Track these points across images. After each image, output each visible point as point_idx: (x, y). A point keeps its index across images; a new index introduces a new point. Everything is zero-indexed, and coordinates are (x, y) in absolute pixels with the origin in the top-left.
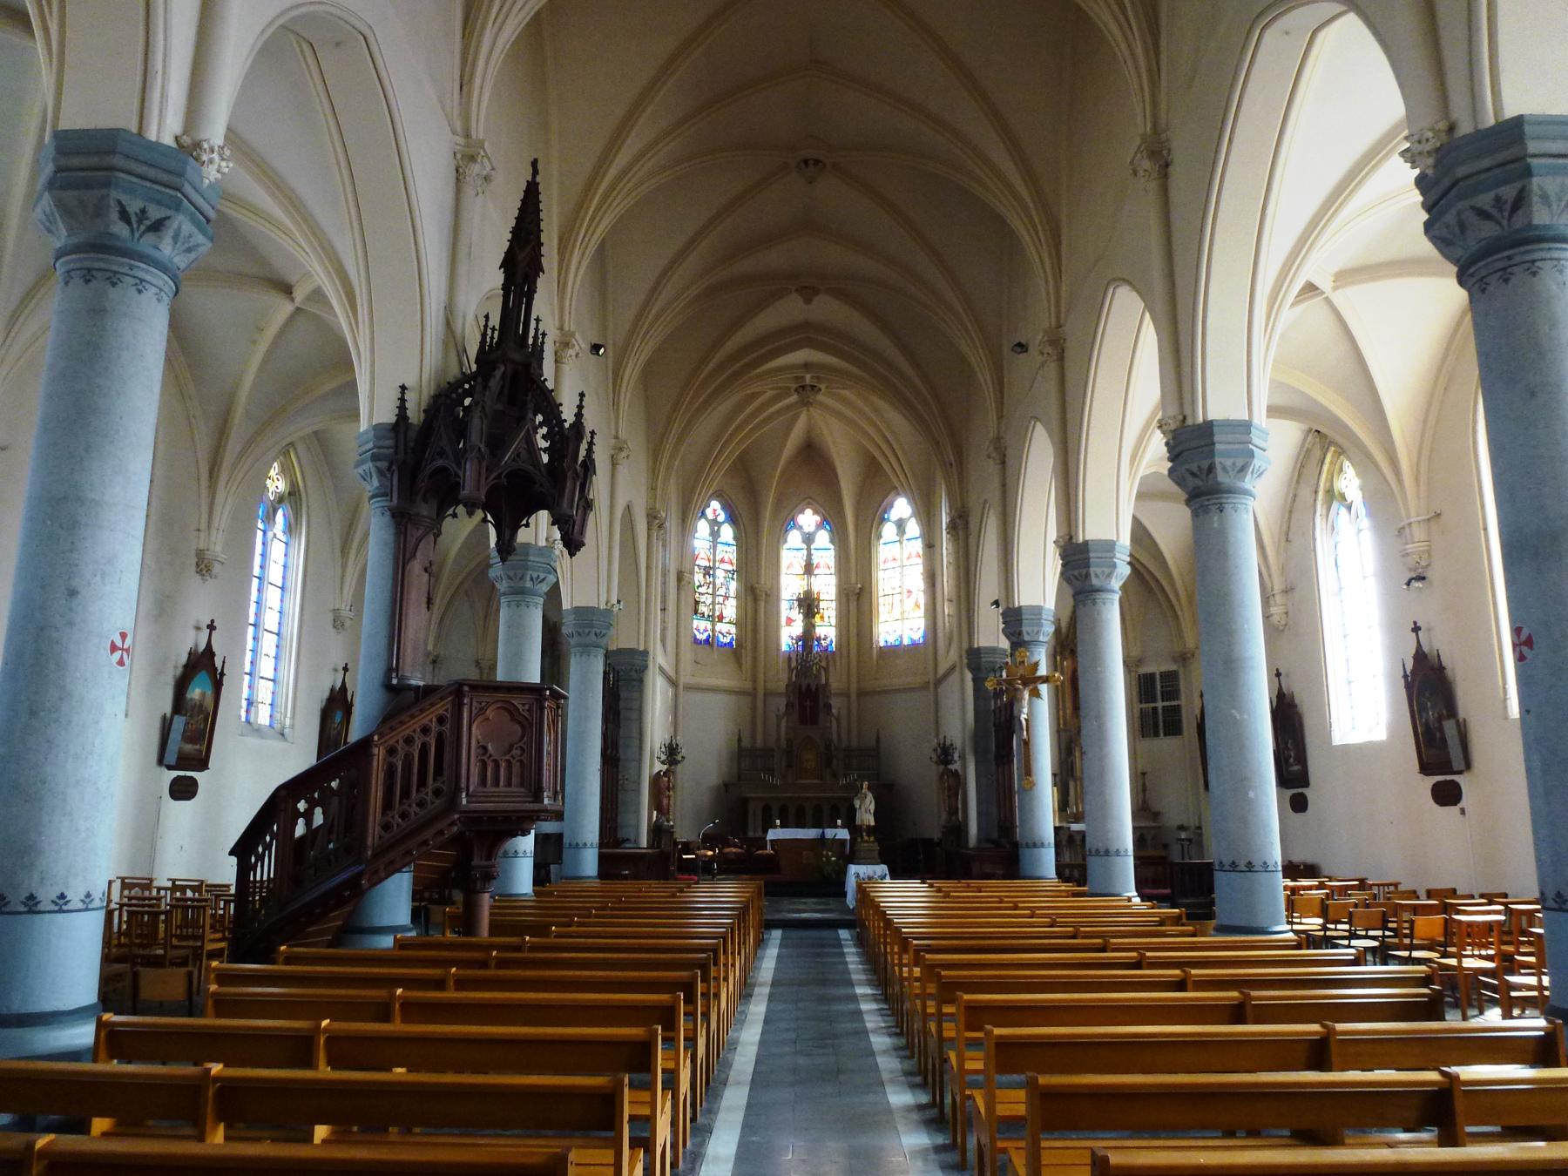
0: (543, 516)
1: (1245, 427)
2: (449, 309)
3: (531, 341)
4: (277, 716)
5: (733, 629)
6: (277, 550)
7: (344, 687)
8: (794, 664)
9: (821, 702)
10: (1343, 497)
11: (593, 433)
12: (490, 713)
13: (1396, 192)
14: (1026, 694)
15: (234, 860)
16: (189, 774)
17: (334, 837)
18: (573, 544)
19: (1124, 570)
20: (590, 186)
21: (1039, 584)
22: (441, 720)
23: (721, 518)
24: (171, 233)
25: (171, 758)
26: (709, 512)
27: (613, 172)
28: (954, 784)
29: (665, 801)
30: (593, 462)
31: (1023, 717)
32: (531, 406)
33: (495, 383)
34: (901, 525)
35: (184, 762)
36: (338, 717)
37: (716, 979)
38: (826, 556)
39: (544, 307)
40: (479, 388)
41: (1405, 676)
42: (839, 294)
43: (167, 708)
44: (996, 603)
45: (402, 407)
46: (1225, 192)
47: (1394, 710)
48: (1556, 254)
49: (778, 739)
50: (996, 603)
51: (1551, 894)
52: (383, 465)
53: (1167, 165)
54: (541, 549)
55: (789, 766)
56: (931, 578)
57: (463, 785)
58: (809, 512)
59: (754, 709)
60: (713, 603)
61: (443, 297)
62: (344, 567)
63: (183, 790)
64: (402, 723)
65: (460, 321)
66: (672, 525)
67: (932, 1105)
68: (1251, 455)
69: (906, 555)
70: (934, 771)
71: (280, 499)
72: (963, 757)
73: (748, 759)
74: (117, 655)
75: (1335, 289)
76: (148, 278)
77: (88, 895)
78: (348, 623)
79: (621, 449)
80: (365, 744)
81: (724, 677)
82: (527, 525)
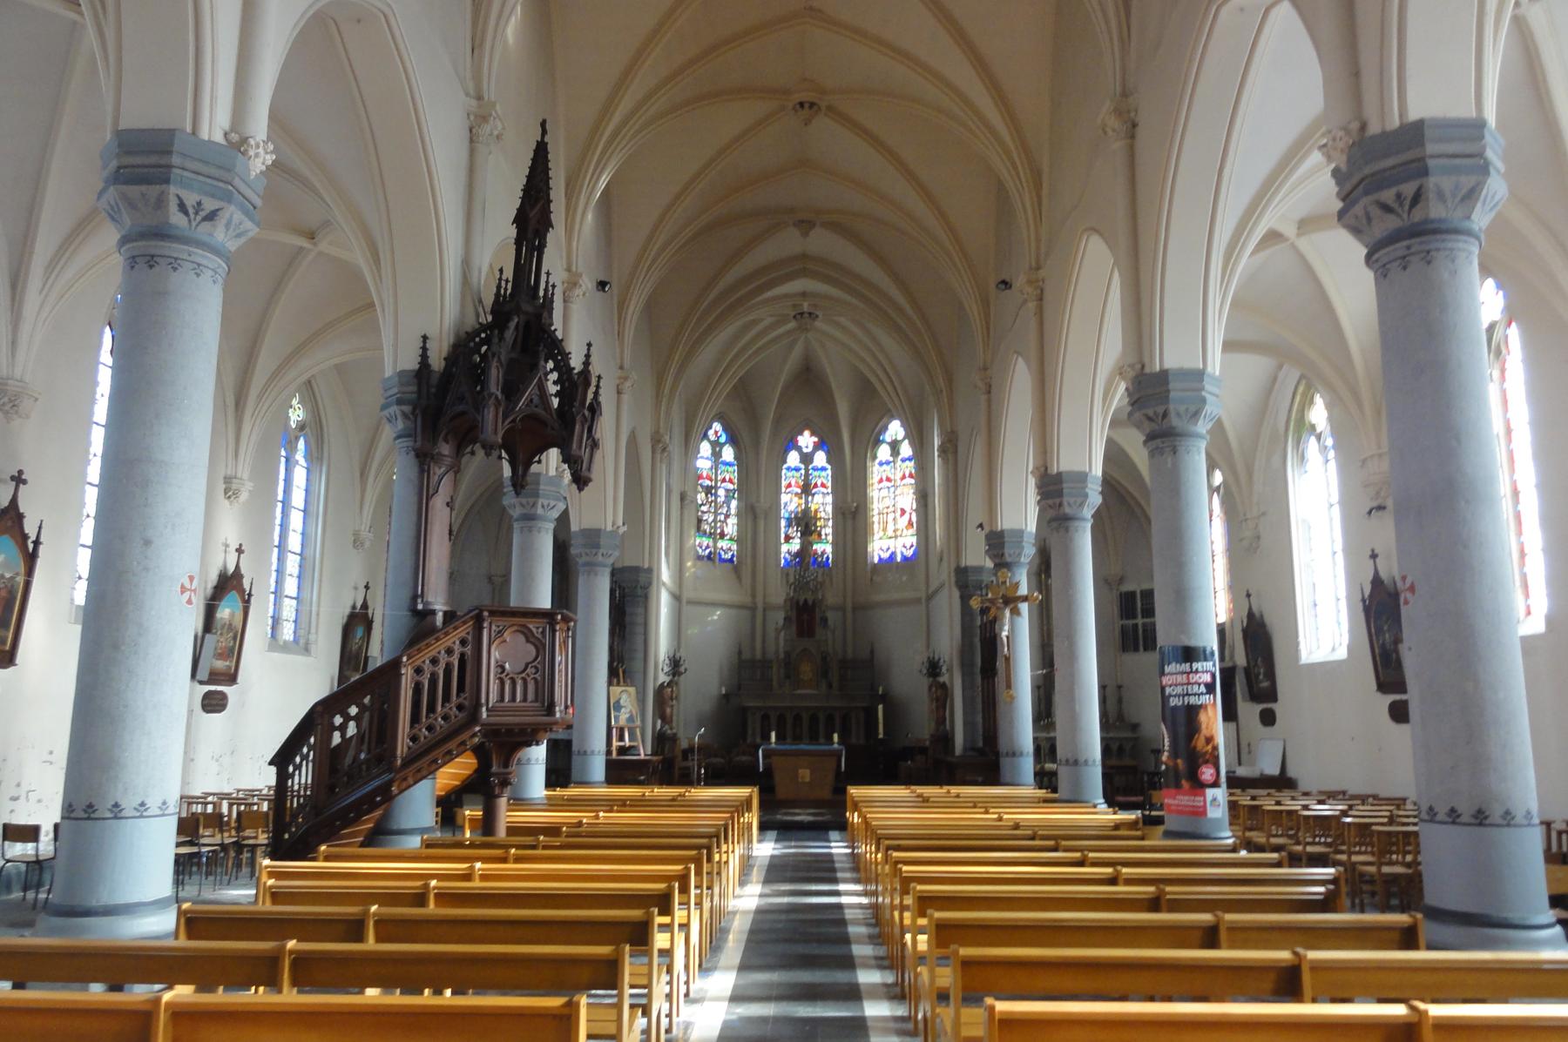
0: (554, 454)
1: (1199, 375)
2: (466, 264)
3: (541, 293)
4: (302, 632)
5: (735, 547)
6: (300, 475)
7: (365, 606)
8: (792, 580)
9: (818, 615)
10: (1313, 427)
11: (599, 377)
13: (1316, 183)
14: (1007, 613)
15: (273, 769)
16: (219, 688)
17: (365, 747)
18: (580, 481)
19: (1095, 498)
20: (596, 129)
21: (1022, 513)
22: (463, 642)
23: (723, 439)
24: (224, 221)
25: (203, 674)
26: (711, 433)
27: (617, 118)
28: (941, 695)
30: (599, 404)
31: (1005, 634)
32: (542, 356)
33: (510, 334)
34: (895, 446)
35: (214, 677)
36: (360, 632)
38: (824, 478)
39: (554, 262)
40: (496, 340)
41: (1364, 600)
44: (981, 526)
46: (1184, 156)
47: (1352, 631)
48: (1449, 245)
49: (777, 652)
50: (981, 526)
51: (1424, 808)
52: (407, 409)
53: (1134, 125)
55: (788, 677)
56: (923, 497)
58: (807, 433)
59: (754, 617)
60: (715, 521)
62: (363, 491)
63: (214, 703)
64: (428, 646)
65: (475, 274)
66: (675, 448)
67: (896, 984)
68: (1204, 401)
69: (899, 475)
70: (925, 682)
71: (302, 427)
72: (950, 670)
73: (748, 670)
74: (187, 595)
75: (1299, 235)
76: (204, 262)
77: (164, 803)
78: (367, 544)
79: (626, 379)
80: (393, 667)
81: (726, 592)
82: (539, 462)
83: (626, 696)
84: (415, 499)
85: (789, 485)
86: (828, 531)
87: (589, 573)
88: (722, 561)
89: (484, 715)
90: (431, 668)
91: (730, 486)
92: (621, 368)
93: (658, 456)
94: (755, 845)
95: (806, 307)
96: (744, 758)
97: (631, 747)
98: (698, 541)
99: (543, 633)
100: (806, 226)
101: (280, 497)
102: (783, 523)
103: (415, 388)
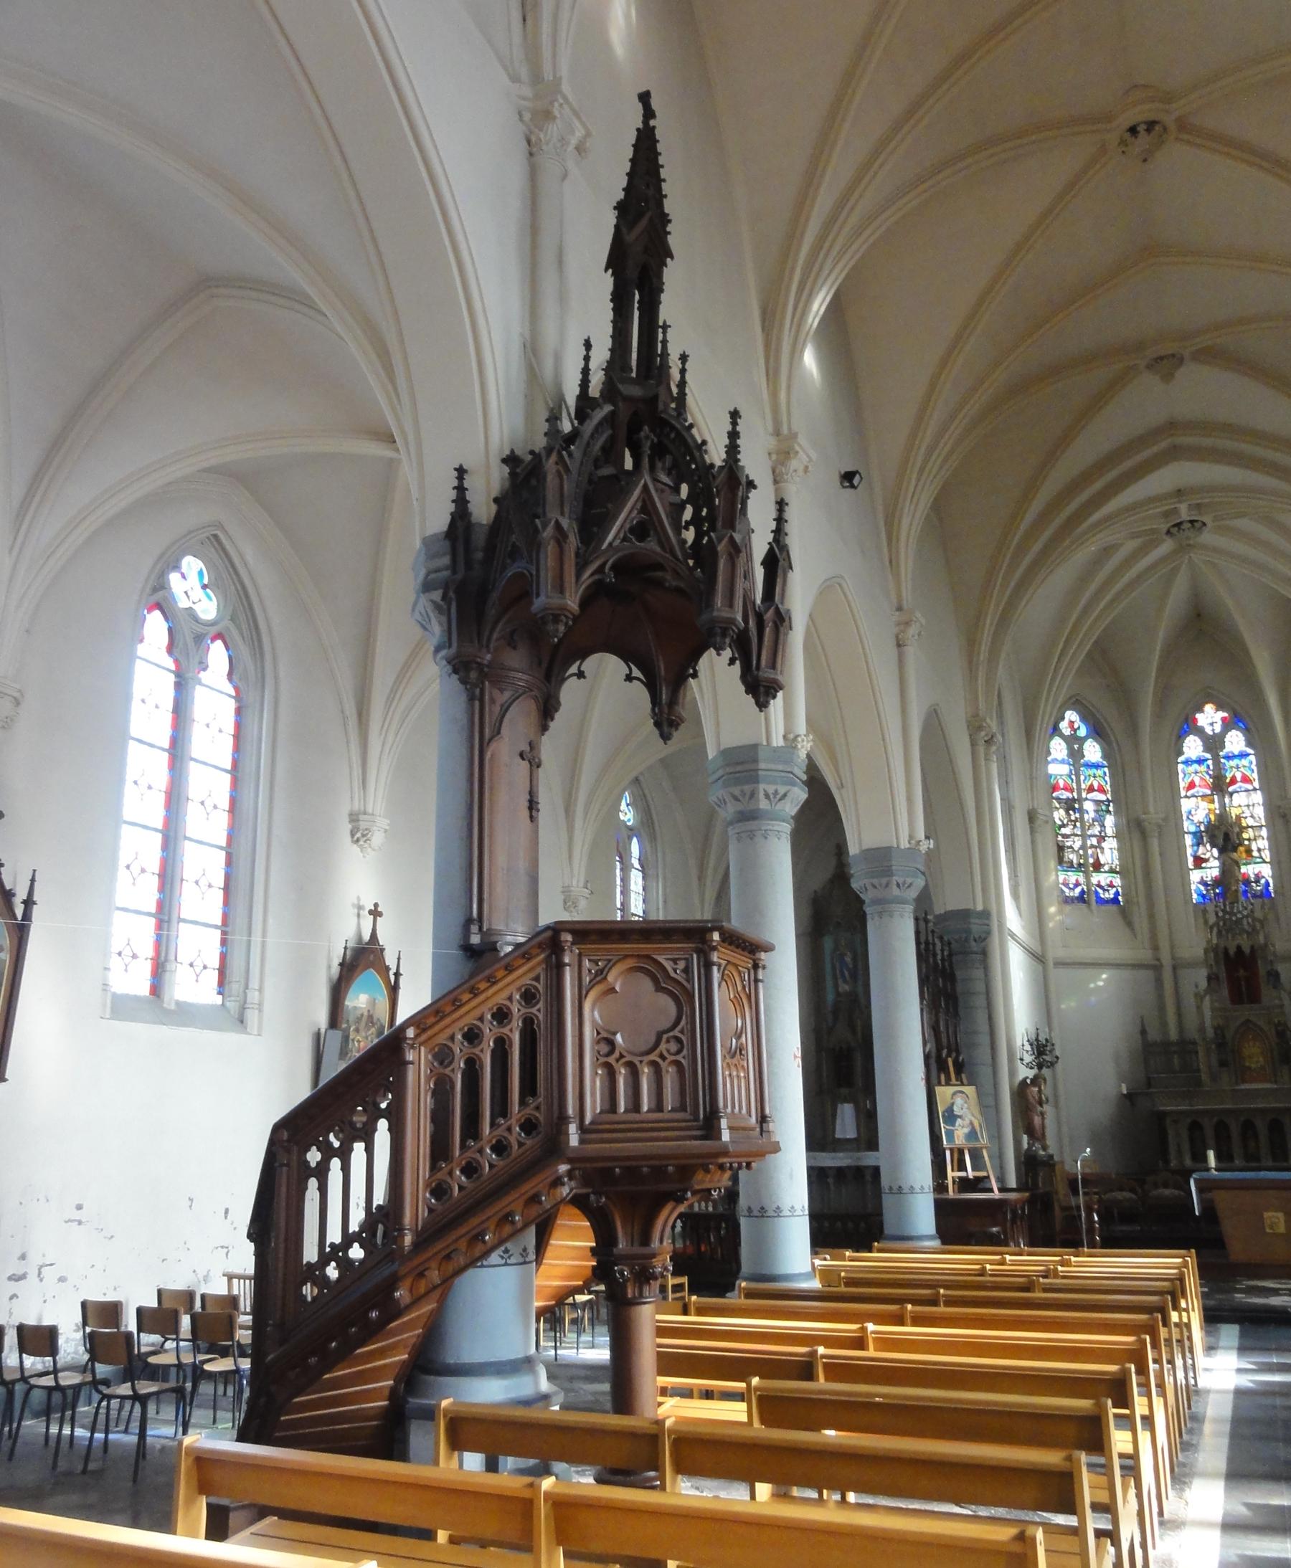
2: (532, 349)
5: (1117, 881)
8: (1212, 920)
9: (1262, 972)
12: (615, 978)
22: (529, 997)
23: (1082, 732)
26: (1064, 726)
29: (1037, 1120)
30: (784, 548)
37: (1186, 1310)
42: (1209, 355)
43: (321, 1017)
45: (461, 500)
49: (1202, 1029)
52: (437, 595)
54: (776, 749)
55: (1223, 1064)
57: (571, 1110)
58: (1209, 708)
59: (1159, 982)
60: (1083, 847)
61: (517, 329)
73: (1160, 1059)
79: (907, 624)
83: (961, 1101)
84: (464, 752)
85: (1192, 785)
86: (1262, 844)
87: (880, 914)
88: (1101, 901)
89: (574, 1141)
90: (468, 1049)
91: (1102, 797)
92: (900, 609)
93: (981, 749)
94: (1201, 1360)
95: (1184, 513)
96: (1167, 1192)
97: (978, 1179)
98: (1061, 878)
99: (687, 970)
100: (1167, 364)
101: (619, 905)
102: (1189, 840)
103: (446, 560)
